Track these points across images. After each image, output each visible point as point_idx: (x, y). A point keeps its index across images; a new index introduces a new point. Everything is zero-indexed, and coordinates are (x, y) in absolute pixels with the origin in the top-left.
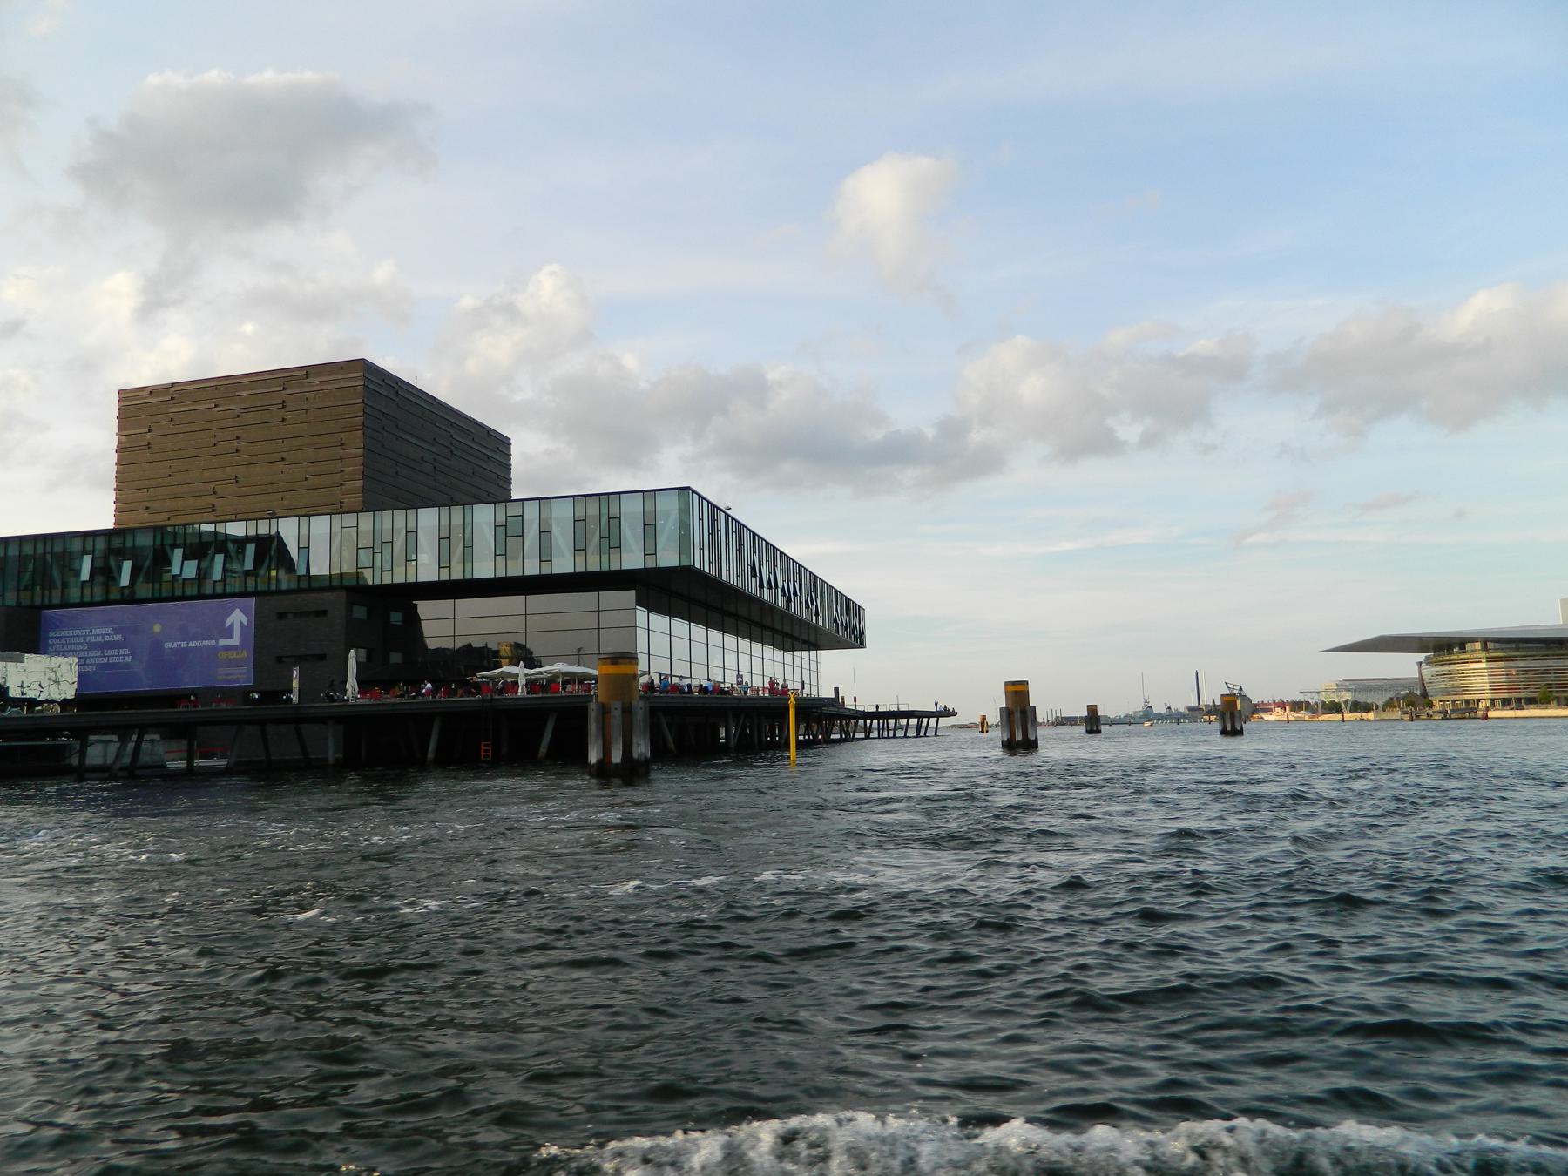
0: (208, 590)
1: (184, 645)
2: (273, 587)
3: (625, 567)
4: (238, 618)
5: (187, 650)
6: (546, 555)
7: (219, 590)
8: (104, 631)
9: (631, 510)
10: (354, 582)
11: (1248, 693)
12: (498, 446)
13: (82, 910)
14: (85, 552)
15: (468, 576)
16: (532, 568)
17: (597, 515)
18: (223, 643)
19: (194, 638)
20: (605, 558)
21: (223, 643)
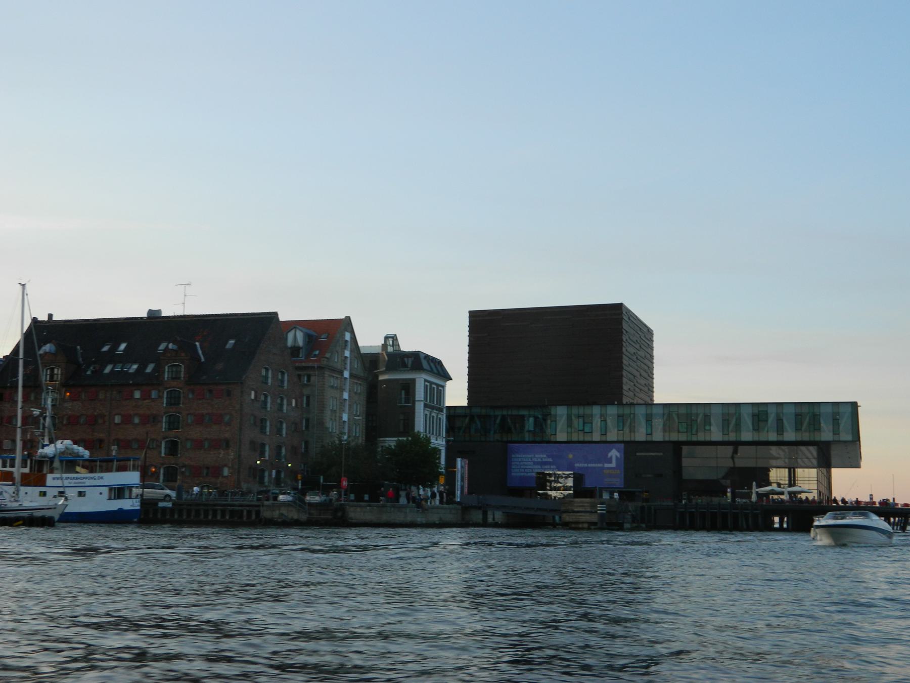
1: (586, 465)
4: (614, 454)
5: (587, 468)
8: (541, 456)
13: (447, 601)
18: (606, 465)
19: (591, 462)
21: (606, 465)
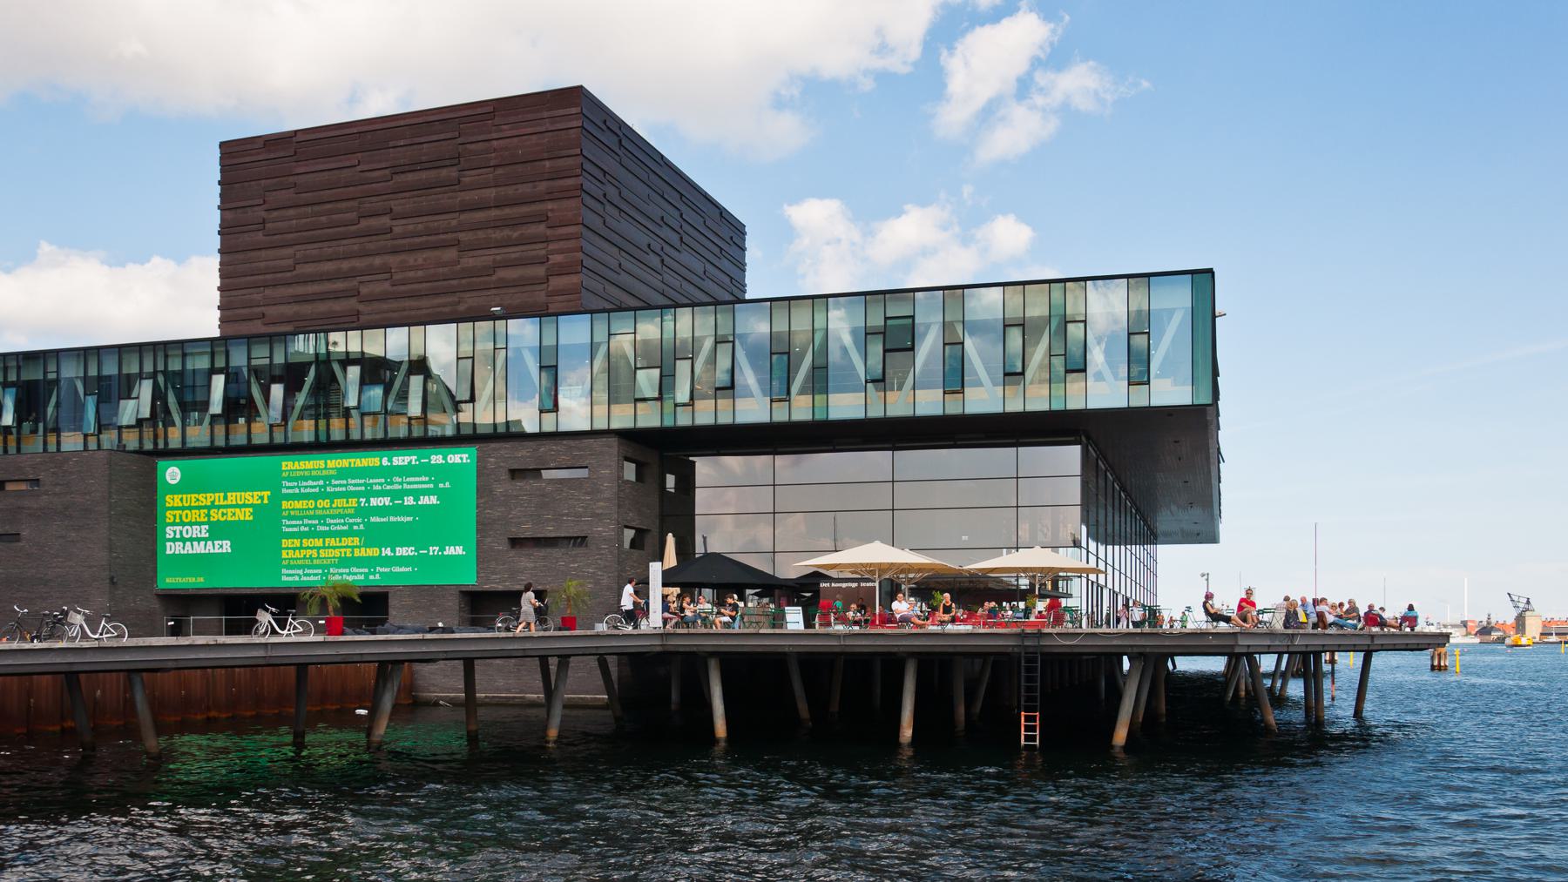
0: (400, 430)
2: (161, 445)
3: (1093, 404)
6: (955, 377)
7: (417, 432)
9: (1106, 309)
10: (490, 430)
11: (1296, 597)
12: (723, 236)
14: (213, 371)
15: (820, 416)
16: (930, 403)
17: (892, 323)
20: (500, 406)
